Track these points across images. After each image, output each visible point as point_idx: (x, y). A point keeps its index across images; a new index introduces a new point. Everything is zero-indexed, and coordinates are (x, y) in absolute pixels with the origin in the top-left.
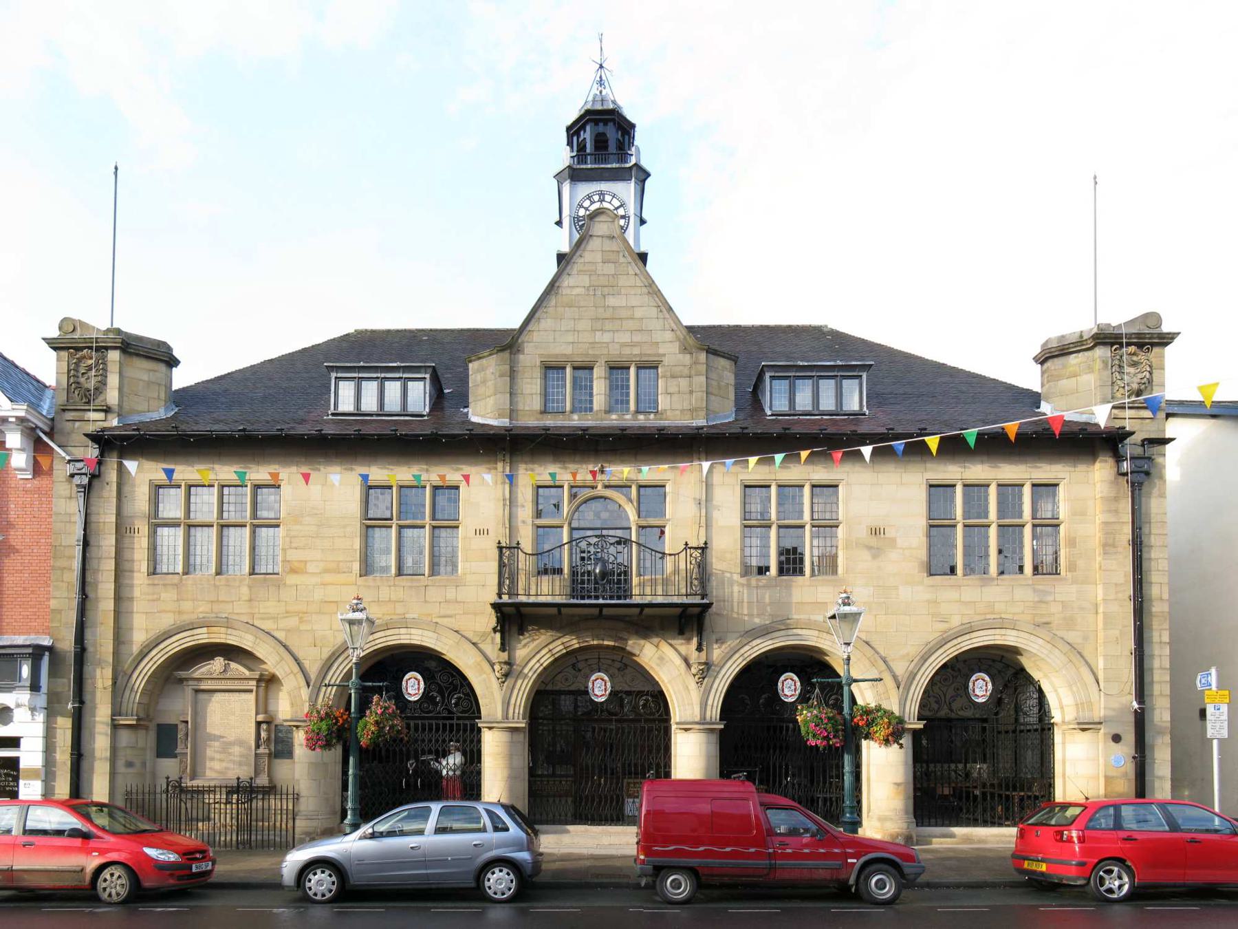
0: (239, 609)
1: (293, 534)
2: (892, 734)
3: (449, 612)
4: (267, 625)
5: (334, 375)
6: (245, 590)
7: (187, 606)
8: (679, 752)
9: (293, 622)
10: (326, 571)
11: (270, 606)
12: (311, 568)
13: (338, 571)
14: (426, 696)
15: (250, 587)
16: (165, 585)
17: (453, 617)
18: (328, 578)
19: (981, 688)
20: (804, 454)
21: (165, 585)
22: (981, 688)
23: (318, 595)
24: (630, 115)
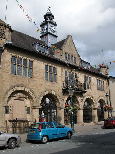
0: (26, 84)
1: (35, 71)
2: (16, 122)
3: (56, 89)
4: (31, 87)
5: (37, 44)
6: (28, 80)
7: (17, 82)
8: (112, 103)
9: (35, 87)
10: (40, 79)
11: (32, 84)
12: (38, 78)
13: (41, 79)
14: (49, 103)
15: (28, 80)
16: (13, 77)
17: (57, 88)
18: (40, 80)
19: (47, 101)
20: (74, 70)
21: (13, 77)
22: (47, 101)
23: (39, 83)
24: (53, 15)
